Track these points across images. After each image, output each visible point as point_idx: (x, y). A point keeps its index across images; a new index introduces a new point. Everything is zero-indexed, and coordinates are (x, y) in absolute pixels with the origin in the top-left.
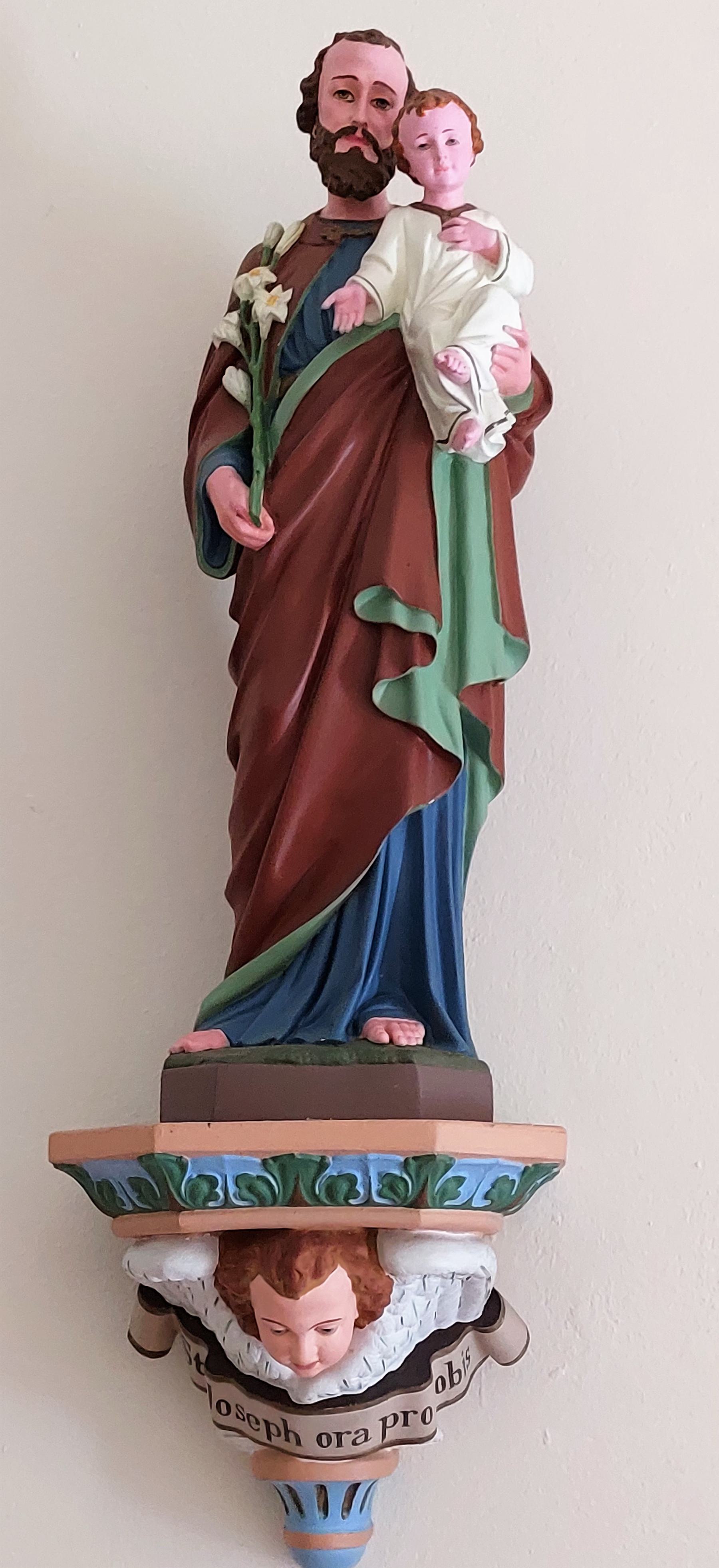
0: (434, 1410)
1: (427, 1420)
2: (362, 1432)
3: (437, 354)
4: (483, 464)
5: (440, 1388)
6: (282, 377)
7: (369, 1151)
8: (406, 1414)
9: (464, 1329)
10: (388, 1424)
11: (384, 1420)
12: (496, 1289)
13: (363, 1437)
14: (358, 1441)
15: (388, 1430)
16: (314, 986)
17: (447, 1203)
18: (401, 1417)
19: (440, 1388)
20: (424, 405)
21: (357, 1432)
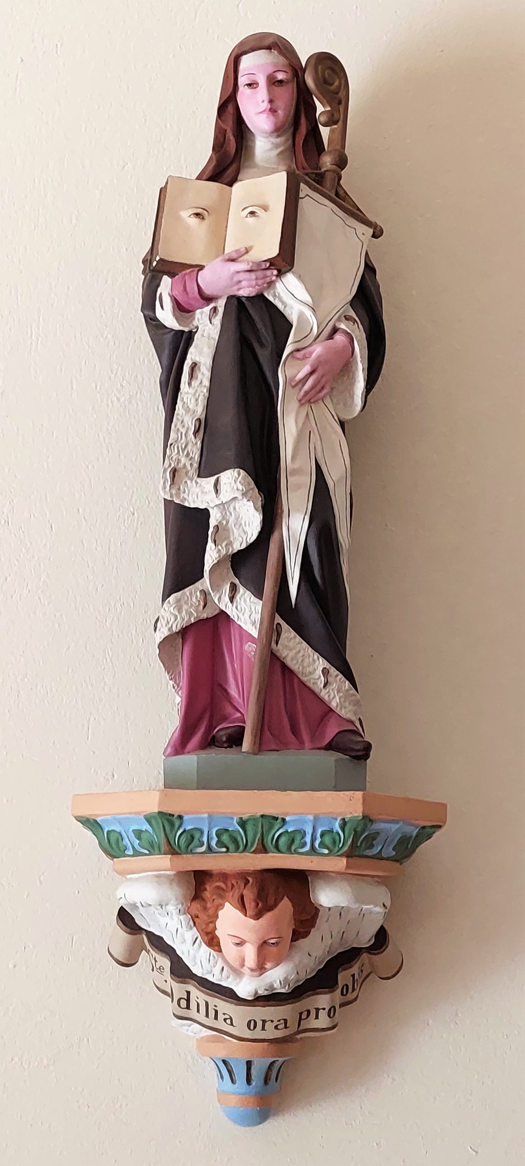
0: (337, 1007)
1: (332, 1015)
2: (282, 1021)
3: (243, 498)
4: (299, 407)
5: (345, 992)
6: (147, 260)
7: (287, 814)
8: (264, 1022)
9: (361, 951)
10: (303, 1017)
11: (301, 1014)
12: (384, 926)
13: (283, 1025)
14: (279, 1027)
15: (302, 1022)
16: (270, 330)
17: (359, 844)
18: (260, 1024)
19: (345, 992)
20: (196, 983)
21: (279, 1021)
